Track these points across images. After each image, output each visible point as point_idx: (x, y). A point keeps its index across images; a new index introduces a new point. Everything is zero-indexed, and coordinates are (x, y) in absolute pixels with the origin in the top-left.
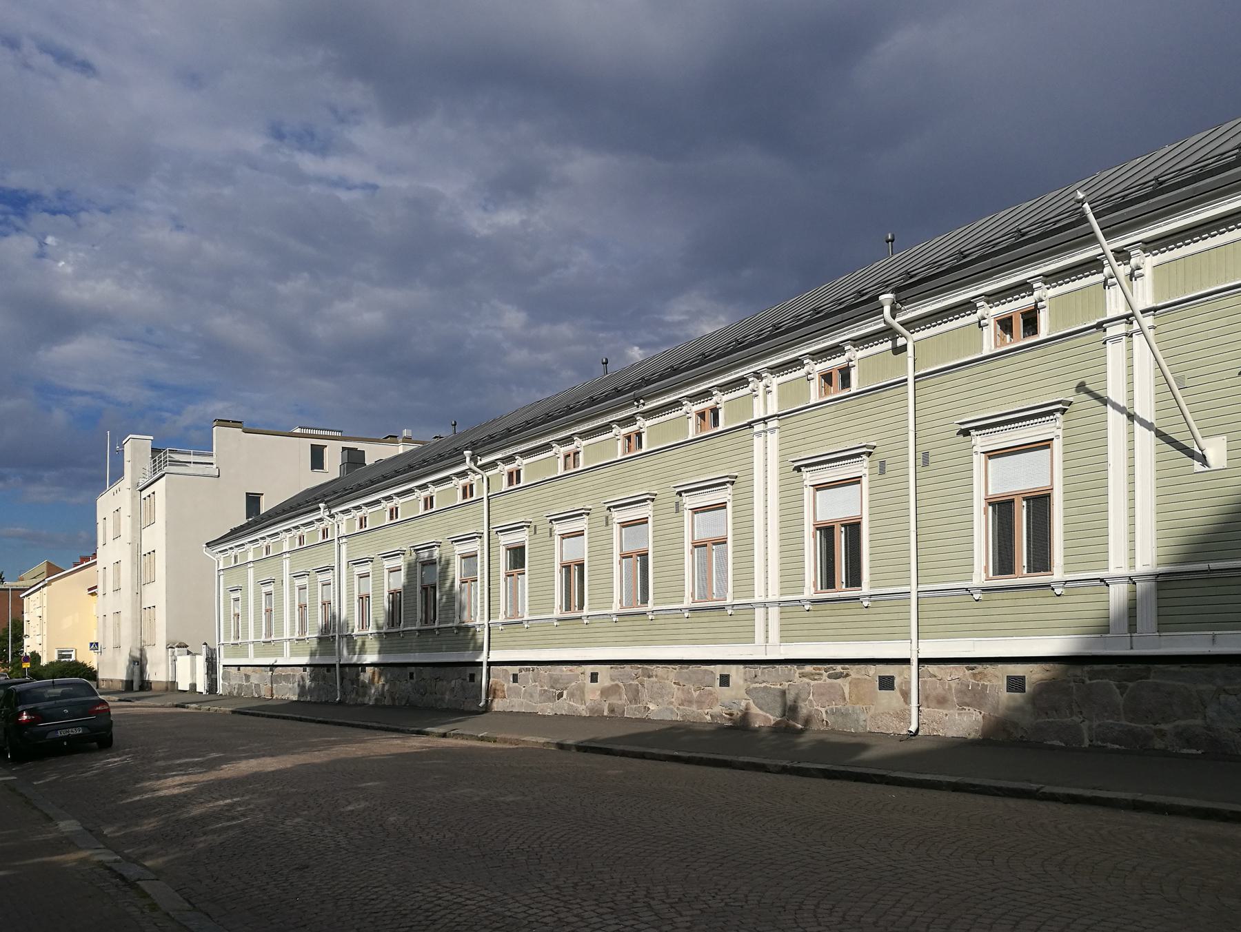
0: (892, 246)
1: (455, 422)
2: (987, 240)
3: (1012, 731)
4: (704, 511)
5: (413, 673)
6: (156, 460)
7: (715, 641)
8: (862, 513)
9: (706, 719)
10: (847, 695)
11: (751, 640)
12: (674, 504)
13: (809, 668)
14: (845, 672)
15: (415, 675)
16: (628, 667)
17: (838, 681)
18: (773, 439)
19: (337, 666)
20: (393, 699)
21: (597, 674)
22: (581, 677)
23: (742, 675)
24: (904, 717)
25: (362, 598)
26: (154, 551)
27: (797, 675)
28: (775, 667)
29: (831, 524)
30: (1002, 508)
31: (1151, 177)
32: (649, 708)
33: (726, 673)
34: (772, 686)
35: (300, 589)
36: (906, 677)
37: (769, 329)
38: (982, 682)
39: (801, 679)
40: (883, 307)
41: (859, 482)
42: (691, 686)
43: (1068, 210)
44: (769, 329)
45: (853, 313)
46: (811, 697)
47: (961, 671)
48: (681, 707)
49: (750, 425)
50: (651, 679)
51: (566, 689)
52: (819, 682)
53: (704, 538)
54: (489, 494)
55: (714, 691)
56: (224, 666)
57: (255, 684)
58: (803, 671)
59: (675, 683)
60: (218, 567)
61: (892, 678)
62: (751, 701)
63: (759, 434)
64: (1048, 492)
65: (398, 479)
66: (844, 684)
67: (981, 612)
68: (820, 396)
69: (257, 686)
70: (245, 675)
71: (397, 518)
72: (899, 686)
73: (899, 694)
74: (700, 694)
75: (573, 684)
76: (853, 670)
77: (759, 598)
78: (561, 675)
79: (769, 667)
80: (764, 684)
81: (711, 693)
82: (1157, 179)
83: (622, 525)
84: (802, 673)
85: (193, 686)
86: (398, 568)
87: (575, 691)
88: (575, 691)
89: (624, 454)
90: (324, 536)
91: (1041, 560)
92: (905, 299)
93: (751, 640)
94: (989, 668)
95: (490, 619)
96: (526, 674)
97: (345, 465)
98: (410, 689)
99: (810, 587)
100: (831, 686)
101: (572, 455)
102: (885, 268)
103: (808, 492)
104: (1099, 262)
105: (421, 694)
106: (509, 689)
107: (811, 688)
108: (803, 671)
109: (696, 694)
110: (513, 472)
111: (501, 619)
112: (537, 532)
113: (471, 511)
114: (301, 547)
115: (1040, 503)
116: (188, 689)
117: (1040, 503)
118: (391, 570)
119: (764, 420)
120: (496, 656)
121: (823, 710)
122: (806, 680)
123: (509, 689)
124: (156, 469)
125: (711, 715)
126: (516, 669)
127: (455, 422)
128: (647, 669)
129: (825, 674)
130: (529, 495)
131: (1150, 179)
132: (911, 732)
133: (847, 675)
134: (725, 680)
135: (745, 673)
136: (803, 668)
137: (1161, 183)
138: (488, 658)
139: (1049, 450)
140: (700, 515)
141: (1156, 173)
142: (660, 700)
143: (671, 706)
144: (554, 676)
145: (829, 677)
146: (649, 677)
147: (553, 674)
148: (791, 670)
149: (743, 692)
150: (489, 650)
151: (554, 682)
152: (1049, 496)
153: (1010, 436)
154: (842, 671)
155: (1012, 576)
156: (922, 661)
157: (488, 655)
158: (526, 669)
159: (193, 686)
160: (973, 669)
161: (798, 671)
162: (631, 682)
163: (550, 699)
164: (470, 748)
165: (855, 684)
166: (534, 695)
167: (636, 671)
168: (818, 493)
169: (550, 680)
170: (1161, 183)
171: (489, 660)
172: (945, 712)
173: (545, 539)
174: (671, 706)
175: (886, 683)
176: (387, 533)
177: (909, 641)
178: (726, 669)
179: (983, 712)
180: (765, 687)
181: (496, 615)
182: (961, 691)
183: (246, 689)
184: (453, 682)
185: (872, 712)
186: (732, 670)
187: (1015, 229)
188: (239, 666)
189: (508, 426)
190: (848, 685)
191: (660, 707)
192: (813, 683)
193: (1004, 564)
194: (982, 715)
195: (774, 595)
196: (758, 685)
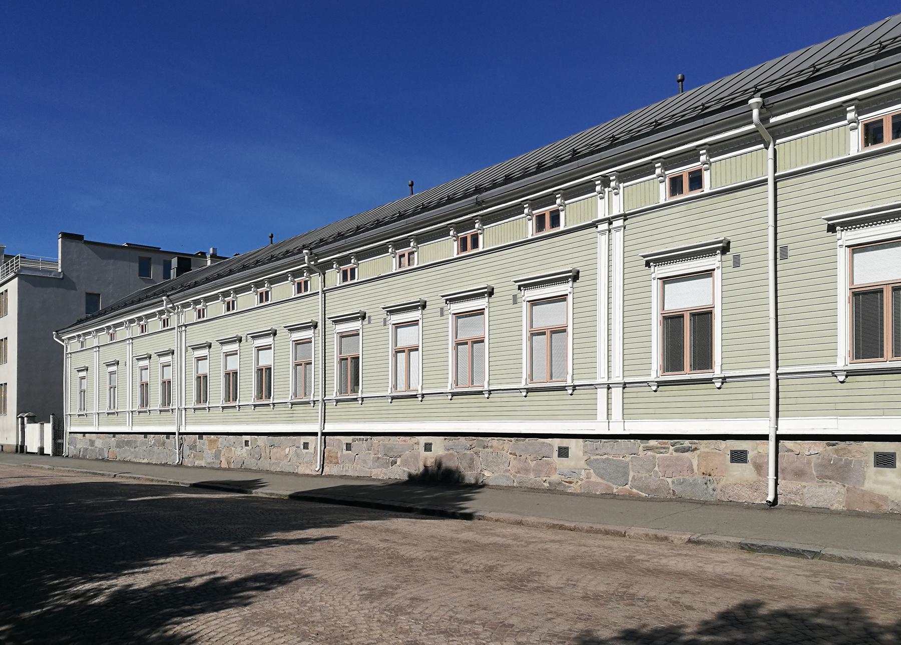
0: (682, 86)
1: (412, 182)
2: (591, 143)
3: (880, 503)
4: (466, 316)
5: (248, 441)
6: (11, 263)
7: (347, 420)
8: (567, 322)
9: (544, 486)
10: (695, 467)
11: (593, 416)
12: (382, 320)
13: (653, 443)
14: (694, 446)
15: (250, 443)
16: (462, 439)
17: (686, 454)
18: (618, 236)
19: (177, 434)
20: (229, 463)
21: (307, 443)
22: (416, 447)
23: (582, 447)
24: (756, 487)
25: (200, 377)
26: (6, 338)
27: (641, 448)
28: (618, 441)
29: (466, 341)
30: (672, 322)
31: (699, 103)
32: (484, 475)
33: (564, 445)
34: (615, 458)
35: (142, 370)
36: (760, 451)
37: (472, 189)
38: (845, 458)
39: (645, 452)
40: (752, 110)
41: (565, 300)
42: (528, 457)
43: (712, 100)
44: (472, 189)
45: (588, 160)
46: (656, 468)
47: (819, 447)
48: (518, 475)
49: (594, 225)
50: (486, 450)
51: (400, 456)
52: (665, 455)
53: (402, 345)
54: (324, 289)
55: (552, 461)
56: (70, 433)
57: (99, 448)
58: (647, 445)
59: (511, 453)
60: (67, 351)
61: (567, 449)
62: (592, 471)
63: (602, 232)
64: (483, 339)
65: (223, 280)
66: (693, 458)
67: (845, 393)
68: (866, 144)
69: (101, 449)
70: (90, 440)
71: (204, 317)
72: (752, 460)
73: (751, 467)
74: (537, 464)
75: (407, 452)
76: (703, 445)
77: (602, 378)
78: (395, 445)
79: (611, 442)
80: (606, 456)
81: (548, 463)
82: (704, 105)
83: (296, 342)
84: (647, 447)
85: (42, 449)
86: (235, 352)
87: (409, 459)
88: (409, 459)
89: (458, 254)
90: (82, 346)
91: (703, 359)
92: (773, 103)
93: (593, 416)
94: (854, 445)
95: (777, 367)
96: (359, 444)
97: (175, 269)
98: (245, 455)
99: (655, 370)
100: (677, 459)
101: (407, 255)
102: (481, 175)
103: (843, 255)
104: (607, 178)
105: (256, 459)
106: (342, 456)
107: (657, 460)
108: (647, 445)
109: (533, 464)
110: (230, 302)
111: (334, 397)
112: (372, 322)
113: (305, 303)
114: (112, 342)
115: (703, 318)
116: (37, 452)
117: (703, 318)
118: (228, 354)
119: (610, 221)
120: (74, 429)
121: (669, 480)
122: (650, 453)
123: (342, 456)
124: (9, 271)
125: (549, 483)
126: (349, 439)
127: (412, 182)
128: (482, 440)
129: (672, 448)
130: (362, 290)
131: (699, 105)
132: (770, 502)
133: (696, 449)
134: (563, 452)
135: (584, 446)
136: (648, 443)
137: (884, 47)
138: (324, 429)
139: (711, 279)
140: (345, 338)
141: (704, 101)
142: (496, 468)
143: (508, 474)
144: (388, 446)
145: (676, 450)
146: (484, 448)
147: (387, 444)
148: (635, 444)
149: (583, 462)
150: (324, 422)
151: (388, 450)
152: (711, 313)
153: (880, 230)
154: (690, 445)
155: (682, 372)
156: (779, 438)
157: (777, 424)
158: (360, 439)
159: (42, 449)
160: (834, 445)
161: (642, 445)
162: (466, 452)
163: (386, 465)
164: (231, 498)
165: (704, 457)
166: (367, 461)
167: (470, 443)
168: (459, 320)
169: (384, 448)
170: (884, 47)
171: (323, 431)
172: (804, 484)
173: (379, 328)
174: (508, 474)
175: (739, 457)
176: (224, 322)
177: (768, 419)
178: (565, 442)
179: (847, 485)
180: (607, 459)
181: (331, 393)
182: (821, 465)
183: (91, 452)
184: (287, 450)
185: (722, 483)
186: (571, 443)
187: (611, 135)
188: (84, 433)
189: (339, 230)
190: (696, 457)
191: (496, 475)
192: (658, 455)
193: (673, 361)
194: (846, 488)
195: (617, 376)
196: (599, 457)
